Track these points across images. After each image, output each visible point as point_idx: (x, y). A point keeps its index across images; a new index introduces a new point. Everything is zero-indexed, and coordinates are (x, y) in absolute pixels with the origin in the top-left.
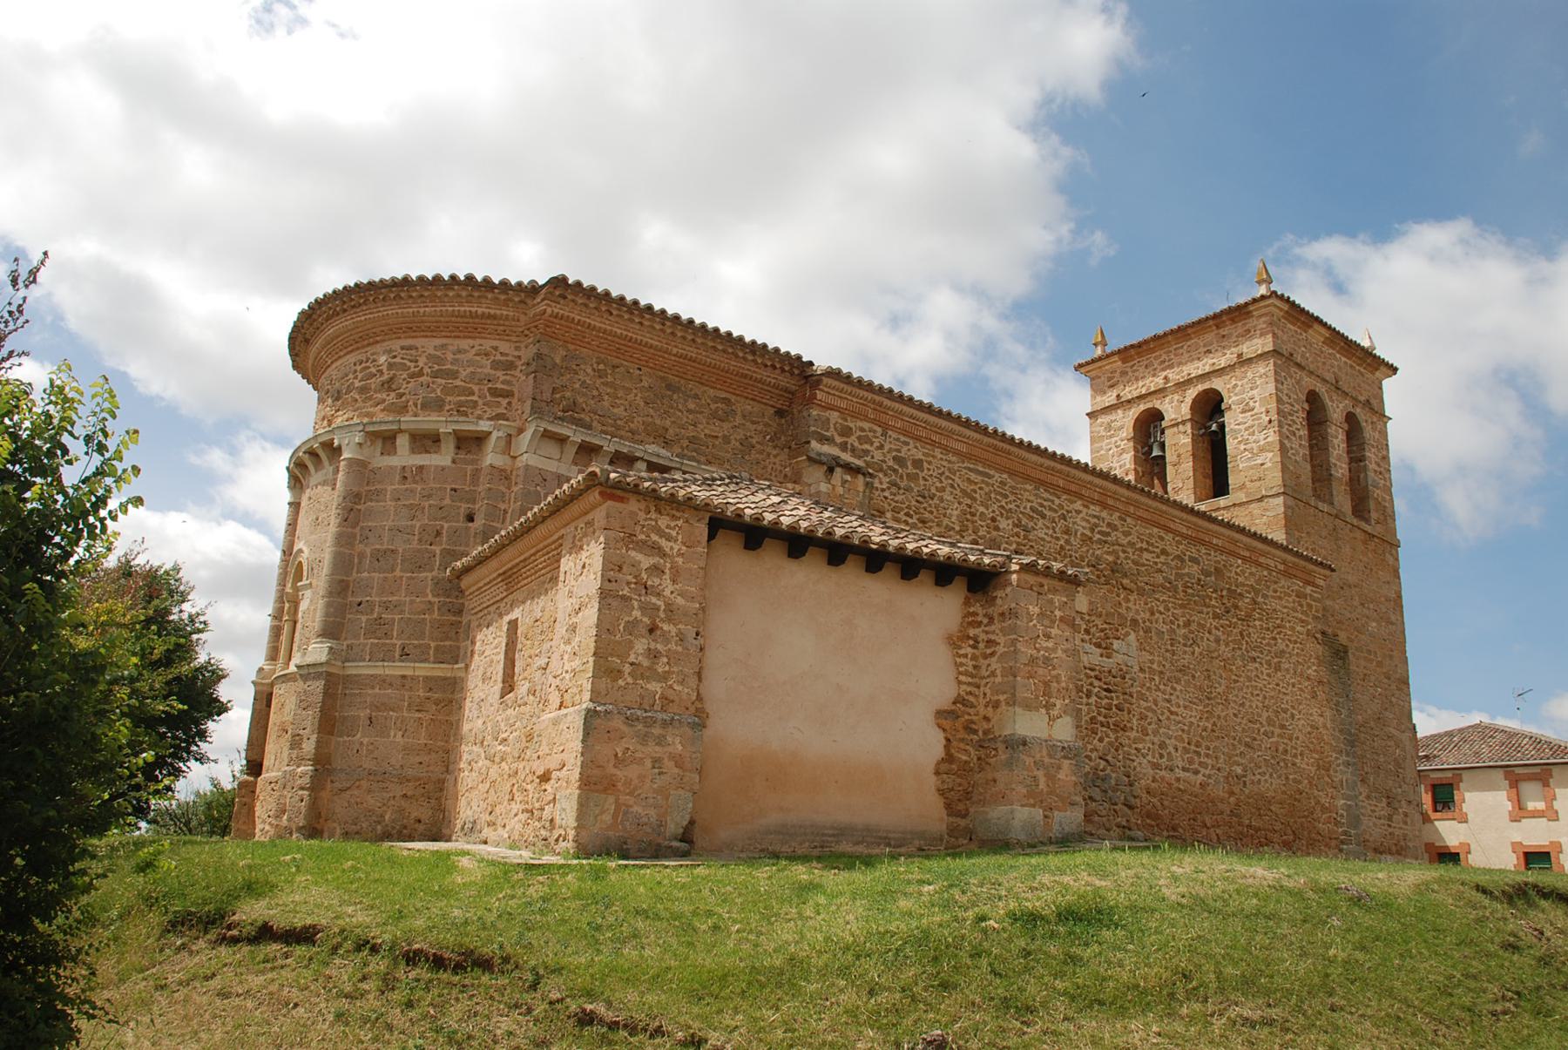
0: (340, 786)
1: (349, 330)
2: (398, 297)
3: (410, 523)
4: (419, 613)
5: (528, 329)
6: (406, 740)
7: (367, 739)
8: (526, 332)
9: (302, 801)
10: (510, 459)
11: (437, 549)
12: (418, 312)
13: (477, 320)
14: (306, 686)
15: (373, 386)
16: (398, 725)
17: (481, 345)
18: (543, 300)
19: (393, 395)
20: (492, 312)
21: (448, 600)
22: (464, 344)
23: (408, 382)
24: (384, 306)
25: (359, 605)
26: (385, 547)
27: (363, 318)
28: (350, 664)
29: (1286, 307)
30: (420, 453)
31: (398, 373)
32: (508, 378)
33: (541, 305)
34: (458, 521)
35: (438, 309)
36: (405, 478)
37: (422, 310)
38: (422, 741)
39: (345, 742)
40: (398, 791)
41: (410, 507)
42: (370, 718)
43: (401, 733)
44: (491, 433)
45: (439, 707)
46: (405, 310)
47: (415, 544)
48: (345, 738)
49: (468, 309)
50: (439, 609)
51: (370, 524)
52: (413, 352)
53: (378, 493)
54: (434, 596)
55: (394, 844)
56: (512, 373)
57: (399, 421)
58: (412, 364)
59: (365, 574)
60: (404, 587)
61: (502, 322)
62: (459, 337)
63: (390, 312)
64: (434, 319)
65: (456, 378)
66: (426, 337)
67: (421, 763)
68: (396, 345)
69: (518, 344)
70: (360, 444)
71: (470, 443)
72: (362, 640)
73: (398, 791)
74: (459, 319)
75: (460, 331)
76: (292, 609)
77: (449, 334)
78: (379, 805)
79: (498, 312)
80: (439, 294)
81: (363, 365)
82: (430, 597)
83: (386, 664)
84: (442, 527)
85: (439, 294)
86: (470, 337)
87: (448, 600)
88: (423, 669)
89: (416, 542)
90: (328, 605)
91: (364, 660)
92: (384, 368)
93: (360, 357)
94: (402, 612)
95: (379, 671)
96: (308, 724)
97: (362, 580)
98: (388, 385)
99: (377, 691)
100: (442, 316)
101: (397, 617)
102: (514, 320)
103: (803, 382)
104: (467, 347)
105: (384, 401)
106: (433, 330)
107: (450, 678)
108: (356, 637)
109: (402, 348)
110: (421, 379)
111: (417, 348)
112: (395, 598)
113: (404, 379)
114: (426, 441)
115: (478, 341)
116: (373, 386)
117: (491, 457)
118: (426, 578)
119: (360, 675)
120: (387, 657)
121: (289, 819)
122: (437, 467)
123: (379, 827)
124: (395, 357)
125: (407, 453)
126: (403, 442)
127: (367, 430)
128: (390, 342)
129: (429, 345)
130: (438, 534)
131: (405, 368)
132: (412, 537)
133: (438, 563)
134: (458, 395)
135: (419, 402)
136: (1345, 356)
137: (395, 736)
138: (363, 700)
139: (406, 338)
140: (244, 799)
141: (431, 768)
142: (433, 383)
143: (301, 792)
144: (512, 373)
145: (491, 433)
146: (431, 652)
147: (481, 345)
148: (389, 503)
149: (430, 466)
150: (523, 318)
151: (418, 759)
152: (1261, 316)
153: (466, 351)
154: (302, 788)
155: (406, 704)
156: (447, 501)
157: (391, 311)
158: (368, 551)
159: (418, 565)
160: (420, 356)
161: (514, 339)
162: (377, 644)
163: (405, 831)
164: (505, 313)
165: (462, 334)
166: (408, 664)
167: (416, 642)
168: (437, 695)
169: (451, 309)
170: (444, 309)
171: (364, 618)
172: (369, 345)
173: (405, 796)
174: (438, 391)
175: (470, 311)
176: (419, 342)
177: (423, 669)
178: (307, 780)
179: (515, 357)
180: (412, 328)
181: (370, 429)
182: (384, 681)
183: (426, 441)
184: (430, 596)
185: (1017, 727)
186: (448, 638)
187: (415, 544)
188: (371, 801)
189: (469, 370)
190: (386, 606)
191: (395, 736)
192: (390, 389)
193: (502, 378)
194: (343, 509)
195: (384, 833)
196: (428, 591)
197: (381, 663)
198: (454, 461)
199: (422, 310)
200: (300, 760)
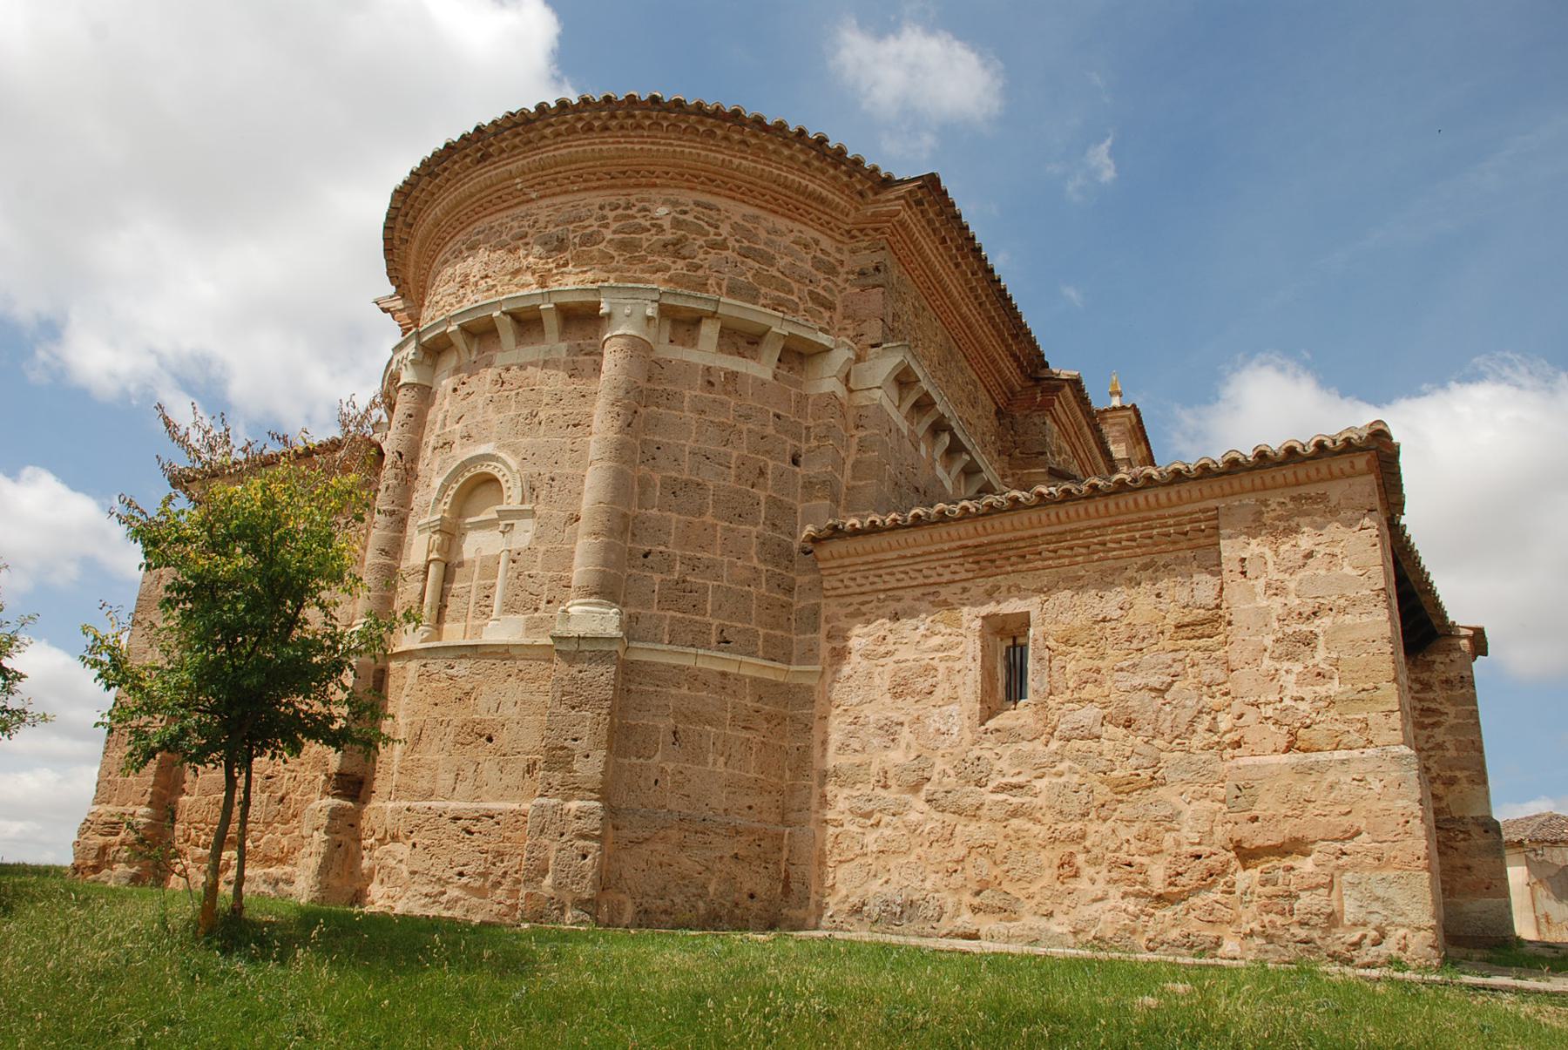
0: (632, 836)
1: (603, 158)
2: (710, 133)
3: (722, 449)
4: (742, 583)
5: (861, 230)
6: (730, 770)
7: (672, 765)
8: (855, 232)
9: (584, 857)
10: (846, 393)
11: (762, 496)
12: (731, 161)
13: (801, 198)
14: (574, 671)
15: (645, 245)
16: (719, 745)
17: (801, 232)
18: (898, 198)
19: (681, 264)
20: (825, 193)
21: (778, 571)
22: (782, 223)
23: (707, 253)
24: (680, 139)
25: (645, 556)
26: (684, 477)
27: (637, 147)
28: (640, 645)
29: (1134, 420)
30: (730, 354)
31: (691, 236)
32: (830, 284)
33: (891, 202)
34: (783, 461)
35: (759, 166)
36: (711, 383)
37: (736, 161)
38: (752, 775)
39: (633, 766)
40: (728, 848)
41: (721, 426)
42: (675, 733)
43: (722, 760)
44: (829, 350)
45: (771, 726)
46: (713, 154)
47: (731, 482)
48: (634, 760)
49: (797, 179)
50: (767, 581)
51: (657, 438)
52: (713, 213)
53: (669, 396)
54: (760, 561)
55: (1027, 949)
56: (835, 279)
57: (719, 301)
58: (712, 230)
59: (654, 512)
60: (719, 541)
61: (828, 210)
62: (775, 212)
63: (687, 150)
64: (748, 178)
65: (772, 266)
66: (734, 198)
67: (750, 808)
68: (688, 198)
69: (840, 245)
70: (649, 319)
71: (798, 355)
72: (655, 610)
73: (728, 848)
74: (780, 189)
75: (780, 206)
76: (446, 543)
77: (764, 204)
78: (699, 868)
79: (830, 196)
80: (771, 147)
81: (620, 211)
82: (755, 562)
83: (701, 652)
84: (766, 465)
85: (771, 147)
86: (790, 218)
87: (778, 571)
88: (752, 667)
89: (733, 479)
90: (608, 548)
91: (661, 641)
92: (667, 224)
93: (613, 199)
94: (718, 577)
95: (688, 662)
96: (586, 733)
97: (649, 519)
98: (675, 248)
99: (685, 690)
100: (761, 177)
101: (710, 584)
102: (842, 212)
103: (1031, 384)
104: (784, 229)
105: (668, 269)
106: (742, 191)
107: (783, 684)
108: (645, 604)
109: (697, 204)
110: (725, 253)
111: (719, 210)
112: (705, 555)
113: (701, 247)
114: (743, 339)
115: (797, 226)
116: (645, 245)
117: (827, 382)
118: (750, 533)
119: (655, 664)
120: (698, 639)
121: (558, 886)
122: (755, 379)
123: (701, 904)
124: (685, 213)
125: (714, 348)
126: (709, 331)
127: (664, 301)
128: (676, 191)
129: (737, 211)
130: (762, 473)
131: (702, 232)
132: (726, 471)
133: (763, 515)
134: (776, 289)
135: (725, 284)
136: (470, 478)
137: (715, 763)
138: (662, 703)
139: (703, 191)
140: (339, 838)
141: (764, 816)
142: (743, 263)
143: (581, 843)
144: (835, 279)
145: (829, 350)
146: (760, 643)
147: (801, 232)
148: (687, 413)
149: (747, 375)
150: (853, 213)
151: (748, 801)
152: (1114, 425)
153: (782, 234)
154: (584, 837)
155: (729, 716)
156: (770, 430)
157: (691, 150)
158: (657, 478)
159: (738, 511)
160: (722, 221)
161: (839, 237)
162: (680, 621)
163: (737, 911)
164: (837, 200)
165: (780, 210)
166: (733, 657)
167: (740, 625)
168: (767, 708)
169: (777, 172)
170: (767, 169)
171: (657, 577)
172: (638, 186)
173: (736, 856)
174: (749, 275)
175: (800, 183)
176: (721, 202)
177: (752, 667)
178: (592, 824)
179: (838, 260)
180: (714, 180)
181: (671, 301)
182: (695, 678)
183: (743, 339)
184: (755, 560)
185: (258, 759)
186: (779, 626)
187: (731, 482)
188: (687, 863)
189: (788, 259)
190: (693, 565)
191: (715, 763)
192: (677, 255)
193: (824, 283)
194: (626, 407)
195: (709, 913)
196: (752, 553)
197: (693, 650)
198: (775, 377)
199: (736, 161)
200: (572, 790)
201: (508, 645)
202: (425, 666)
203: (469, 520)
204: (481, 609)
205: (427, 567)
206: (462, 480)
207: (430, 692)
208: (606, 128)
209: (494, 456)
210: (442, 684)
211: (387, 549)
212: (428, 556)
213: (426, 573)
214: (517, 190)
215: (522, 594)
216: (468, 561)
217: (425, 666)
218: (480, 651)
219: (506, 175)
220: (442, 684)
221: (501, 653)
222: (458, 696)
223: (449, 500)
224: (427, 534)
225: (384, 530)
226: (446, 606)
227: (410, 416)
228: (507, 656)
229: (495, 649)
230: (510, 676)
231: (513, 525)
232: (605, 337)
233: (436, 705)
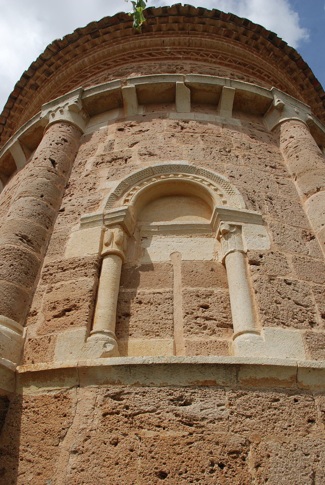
201: (297, 369)
202: (116, 397)
203: (154, 224)
204: (198, 320)
205: (100, 262)
206: (147, 185)
207: (141, 447)
208: (237, 39)
209: (194, 168)
210: (170, 433)
211: (30, 237)
212: (101, 248)
213: (99, 267)
214: (166, 52)
215: (284, 302)
216: (160, 265)
217: (116, 397)
218: (243, 376)
219: (159, 42)
220: (170, 433)
221: (283, 382)
222: (217, 458)
223: (132, 199)
224: (97, 229)
225: (29, 217)
226: (128, 315)
227: (66, 141)
228: (294, 386)
229: (274, 375)
230: (311, 421)
231: (240, 227)
232: (280, 121)
233: (163, 475)
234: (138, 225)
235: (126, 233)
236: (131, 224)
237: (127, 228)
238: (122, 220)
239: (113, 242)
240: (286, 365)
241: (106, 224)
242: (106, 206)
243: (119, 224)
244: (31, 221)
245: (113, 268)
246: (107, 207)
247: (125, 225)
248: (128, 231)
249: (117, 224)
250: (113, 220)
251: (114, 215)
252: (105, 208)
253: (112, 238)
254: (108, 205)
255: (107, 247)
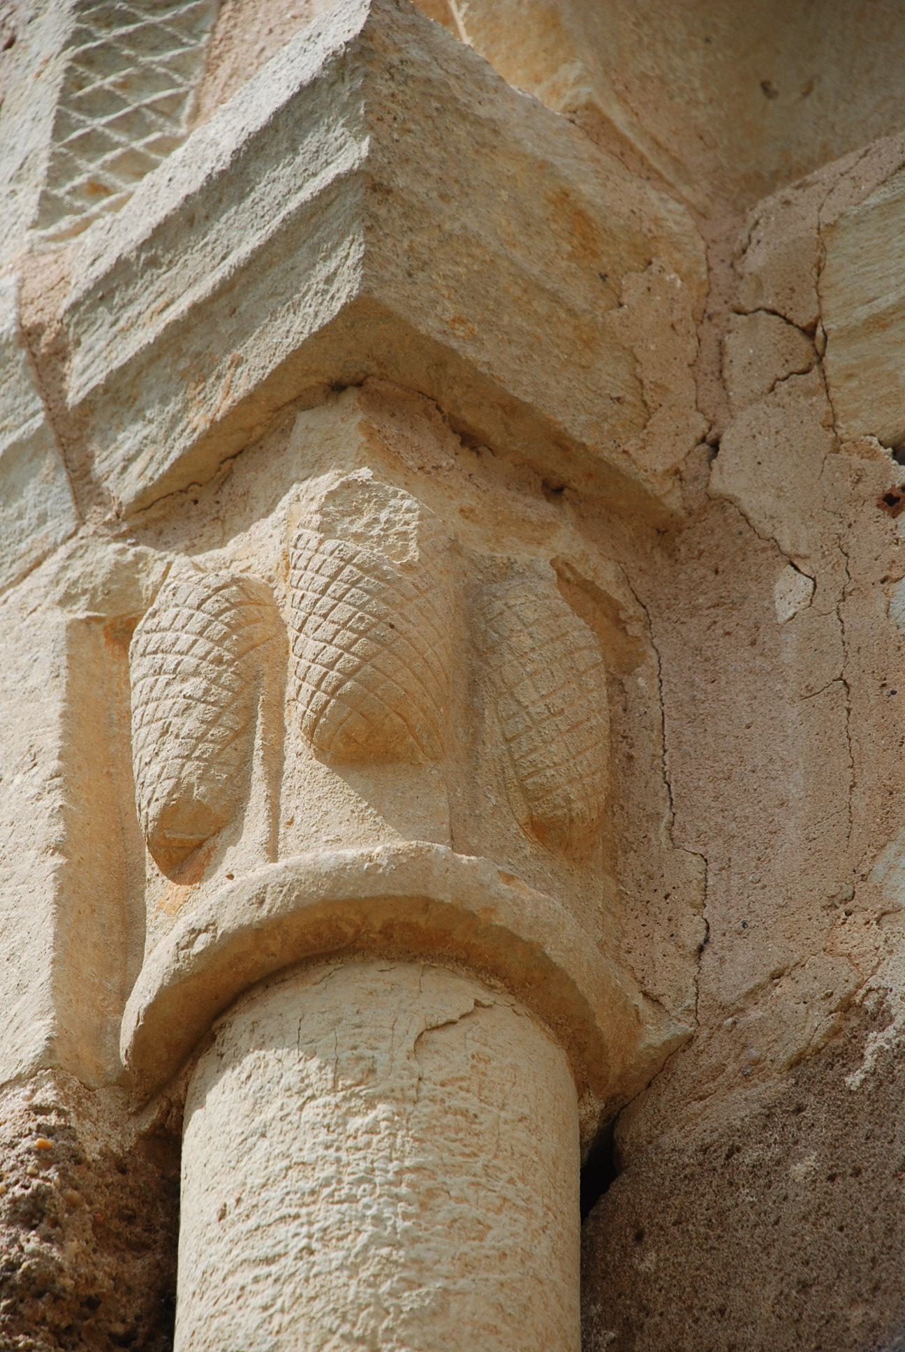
234: (756, 259)
235: (554, 491)
236: (578, 294)
237: (512, 409)
238: (346, 288)
239: (275, 756)
240: (577, 1278)
241: (126, 488)
242: (60, 170)
243: (337, 388)
244: (402, 1225)
245: (325, 1214)
246: (90, 168)
247: (442, 358)
248: (561, 442)
249: (303, 402)
250: (201, 370)
251: (195, 258)
252: (49, 209)
253: (249, 679)
254: (92, 144)
255: (197, 878)
